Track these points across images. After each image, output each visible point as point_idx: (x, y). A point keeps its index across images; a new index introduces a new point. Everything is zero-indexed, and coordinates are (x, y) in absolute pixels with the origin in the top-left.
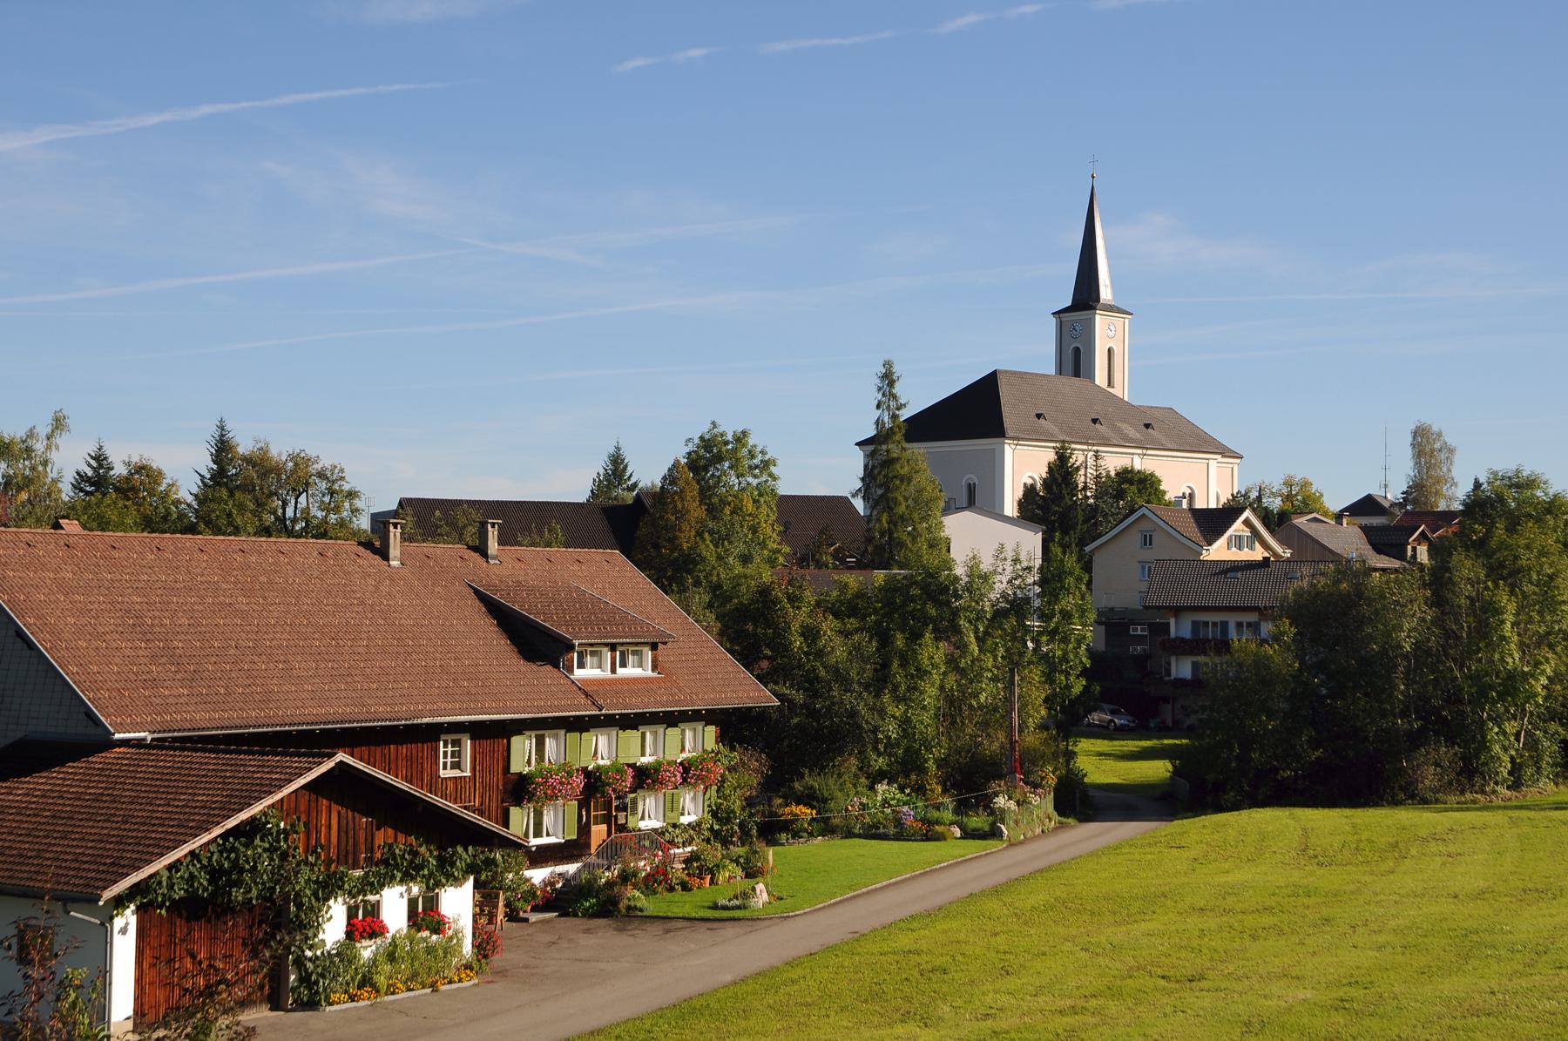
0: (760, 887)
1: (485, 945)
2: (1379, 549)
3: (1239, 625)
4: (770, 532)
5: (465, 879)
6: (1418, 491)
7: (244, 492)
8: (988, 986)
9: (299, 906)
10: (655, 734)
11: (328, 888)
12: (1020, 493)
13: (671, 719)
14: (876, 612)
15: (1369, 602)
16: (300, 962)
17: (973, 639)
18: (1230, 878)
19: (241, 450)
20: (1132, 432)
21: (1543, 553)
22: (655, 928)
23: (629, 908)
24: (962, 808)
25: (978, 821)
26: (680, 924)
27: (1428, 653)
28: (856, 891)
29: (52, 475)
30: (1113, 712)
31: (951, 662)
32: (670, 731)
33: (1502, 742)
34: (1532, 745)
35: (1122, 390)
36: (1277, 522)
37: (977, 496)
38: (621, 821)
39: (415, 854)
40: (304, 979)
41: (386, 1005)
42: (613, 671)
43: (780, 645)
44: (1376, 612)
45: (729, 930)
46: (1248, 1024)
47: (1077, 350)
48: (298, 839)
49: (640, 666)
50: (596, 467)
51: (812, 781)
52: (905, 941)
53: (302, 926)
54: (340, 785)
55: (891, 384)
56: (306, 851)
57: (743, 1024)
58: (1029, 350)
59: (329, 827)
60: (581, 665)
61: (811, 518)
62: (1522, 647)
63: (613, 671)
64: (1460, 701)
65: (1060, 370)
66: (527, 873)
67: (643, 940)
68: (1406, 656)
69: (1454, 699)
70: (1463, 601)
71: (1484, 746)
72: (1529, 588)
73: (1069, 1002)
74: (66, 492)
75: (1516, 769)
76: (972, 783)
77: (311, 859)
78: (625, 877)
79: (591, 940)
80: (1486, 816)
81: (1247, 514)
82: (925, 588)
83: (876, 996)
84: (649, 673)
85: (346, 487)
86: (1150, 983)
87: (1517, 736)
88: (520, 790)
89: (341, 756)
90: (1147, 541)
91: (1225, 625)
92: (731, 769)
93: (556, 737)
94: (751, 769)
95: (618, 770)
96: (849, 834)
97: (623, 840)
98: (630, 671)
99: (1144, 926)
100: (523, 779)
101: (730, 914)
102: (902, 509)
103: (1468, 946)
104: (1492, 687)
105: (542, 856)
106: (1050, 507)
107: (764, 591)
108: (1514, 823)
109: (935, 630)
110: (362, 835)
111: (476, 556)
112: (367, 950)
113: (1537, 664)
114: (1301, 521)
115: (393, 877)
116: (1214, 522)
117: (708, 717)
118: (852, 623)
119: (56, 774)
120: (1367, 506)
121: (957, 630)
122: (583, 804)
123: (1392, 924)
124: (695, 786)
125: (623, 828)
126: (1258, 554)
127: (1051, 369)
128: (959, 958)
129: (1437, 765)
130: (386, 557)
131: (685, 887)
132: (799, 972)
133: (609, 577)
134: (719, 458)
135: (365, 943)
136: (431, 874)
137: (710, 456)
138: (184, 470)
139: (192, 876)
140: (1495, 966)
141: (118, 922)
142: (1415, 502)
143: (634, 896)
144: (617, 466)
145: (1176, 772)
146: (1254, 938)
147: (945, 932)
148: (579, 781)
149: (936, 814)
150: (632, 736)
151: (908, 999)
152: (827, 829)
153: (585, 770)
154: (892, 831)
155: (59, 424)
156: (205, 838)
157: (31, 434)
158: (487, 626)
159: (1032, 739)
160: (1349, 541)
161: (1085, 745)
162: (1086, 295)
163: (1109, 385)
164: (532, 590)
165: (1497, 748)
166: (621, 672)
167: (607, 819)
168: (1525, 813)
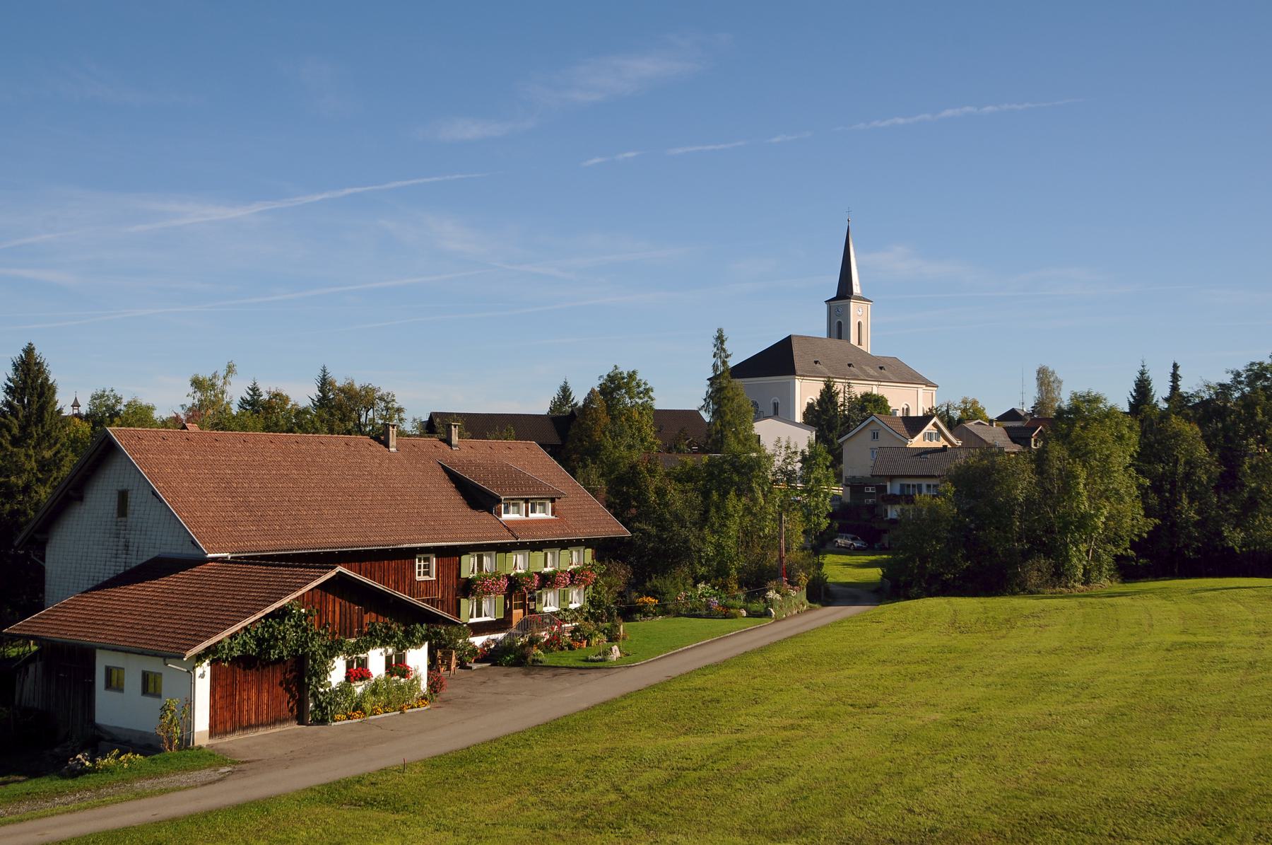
0: (615, 648)
1: (435, 685)
2: (1014, 440)
3: (929, 486)
4: (650, 432)
5: (422, 644)
6: (1040, 405)
7: (341, 410)
8: (743, 711)
9: (314, 661)
10: (553, 554)
11: (332, 650)
12: (804, 409)
13: (564, 545)
14: (703, 479)
15: (999, 472)
16: (315, 695)
17: (760, 495)
18: (905, 641)
19: (337, 384)
20: (871, 372)
21: (1103, 441)
22: (548, 673)
23: (534, 661)
24: (750, 597)
25: (758, 606)
26: (564, 671)
27: (1034, 502)
28: (685, 650)
29: (227, 399)
30: (853, 539)
31: (748, 510)
32: (563, 552)
33: (1078, 557)
34: (1097, 558)
35: (866, 347)
36: (953, 424)
37: (780, 411)
38: (532, 607)
39: (389, 629)
40: (318, 706)
41: (369, 722)
42: (527, 515)
43: (641, 498)
44: (1002, 478)
45: (593, 675)
46: (896, 736)
47: (840, 323)
48: (314, 619)
49: (544, 512)
50: (554, 393)
51: (656, 582)
52: (698, 682)
53: (316, 674)
54: (339, 586)
55: (722, 342)
56: (319, 627)
57: (586, 735)
58: (814, 325)
59: (334, 612)
60: (507, 511)
61: (676, 425)
62: (1089, 498)
63: (527, 515)
64: (1053, 532)
65: (830, 335)
66: (472, 639)
67: (539, 681)
68: (1020, 505)
69: (1049, 531)
70: (1055, 471)
71: (1067, 559)
72: (1094, 463)
73: (791, 721)
74: (235, 410)
75: (1086, 572)
76: (756, 583)
77: (322, 632)
78: (533, 642)
79: (508, 681)
80: (1065, 602)
81: (935, 419)
82: (733, 465)
83: (673, 718)
84: (550, 516)
85: (396, 406)
86: (842, 708)
87: (1088, 552)
88: (467, 588)
89: (340, 569)
90: (875, 436)
91: (920, 486)
92: (602, 575)
93: (490, 556)
94: (622, 573)
95: (529, 576)
96: (678, 615)
97: (534, 619)
98: (538, 515)
99: (847, 672)
100: (469, 582)
101: (598, 665)
102: (728, 417)
103: (1041, 683)
104: (1072, 523)
105: (479, 629)
106: (822, 417)
107: (633, 467)
108: (1081, 606)
109: (739, 489)
110: (355, 617)
111: (445, 445)
112: (359, 688)
113: (1098, 509)
114: (970, 425)
115: (375, 643)
116: (914, 424)
117: (587, 543)
118: (689, 486)
119: (172, 579)
120: (1012, 415)
121: (751, 490)
122: (508, 597)
123: (998, 670)
124: (578, 585)
125: (533, 612)
126: (941, 443)
127: (825, 336)
128: (729, 693)
129: (1039, 570)
130: (387, 446)
131: (571, 648)
132: (629, 702)
133: (532, 460)
134: (619, 388)
135: (358, 683)
136: (400, 641)
137: (614, 386)
138: (303, 394)
139: (245, 642)
140: (1055, 697)
141: (199, 671)
142: (1039, 413)
143: (537, 652)
144: (565, 392)
145: (884, 576)
146: (912, 679)
147: (725, 676)
148: (504, 583)
149: (731, 602)
150: (539, 555)
151: (692, 720)
152: (664, 611)
153: (508, 576)
154: (704, 612)
155: (230, 369)
156: (252, 619)
157: (215, 376)
158: (449, 487)
159: (796, 555)
160: (997, 437)
161: (829, 559)
162: (845, 290)
163: (859, 343)
164: (478, 466)
165: (1075, 560)
166: (532, 516)
167: (523, 606)
168: (1089, 600)
